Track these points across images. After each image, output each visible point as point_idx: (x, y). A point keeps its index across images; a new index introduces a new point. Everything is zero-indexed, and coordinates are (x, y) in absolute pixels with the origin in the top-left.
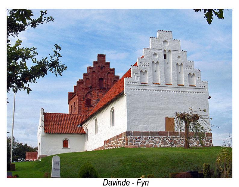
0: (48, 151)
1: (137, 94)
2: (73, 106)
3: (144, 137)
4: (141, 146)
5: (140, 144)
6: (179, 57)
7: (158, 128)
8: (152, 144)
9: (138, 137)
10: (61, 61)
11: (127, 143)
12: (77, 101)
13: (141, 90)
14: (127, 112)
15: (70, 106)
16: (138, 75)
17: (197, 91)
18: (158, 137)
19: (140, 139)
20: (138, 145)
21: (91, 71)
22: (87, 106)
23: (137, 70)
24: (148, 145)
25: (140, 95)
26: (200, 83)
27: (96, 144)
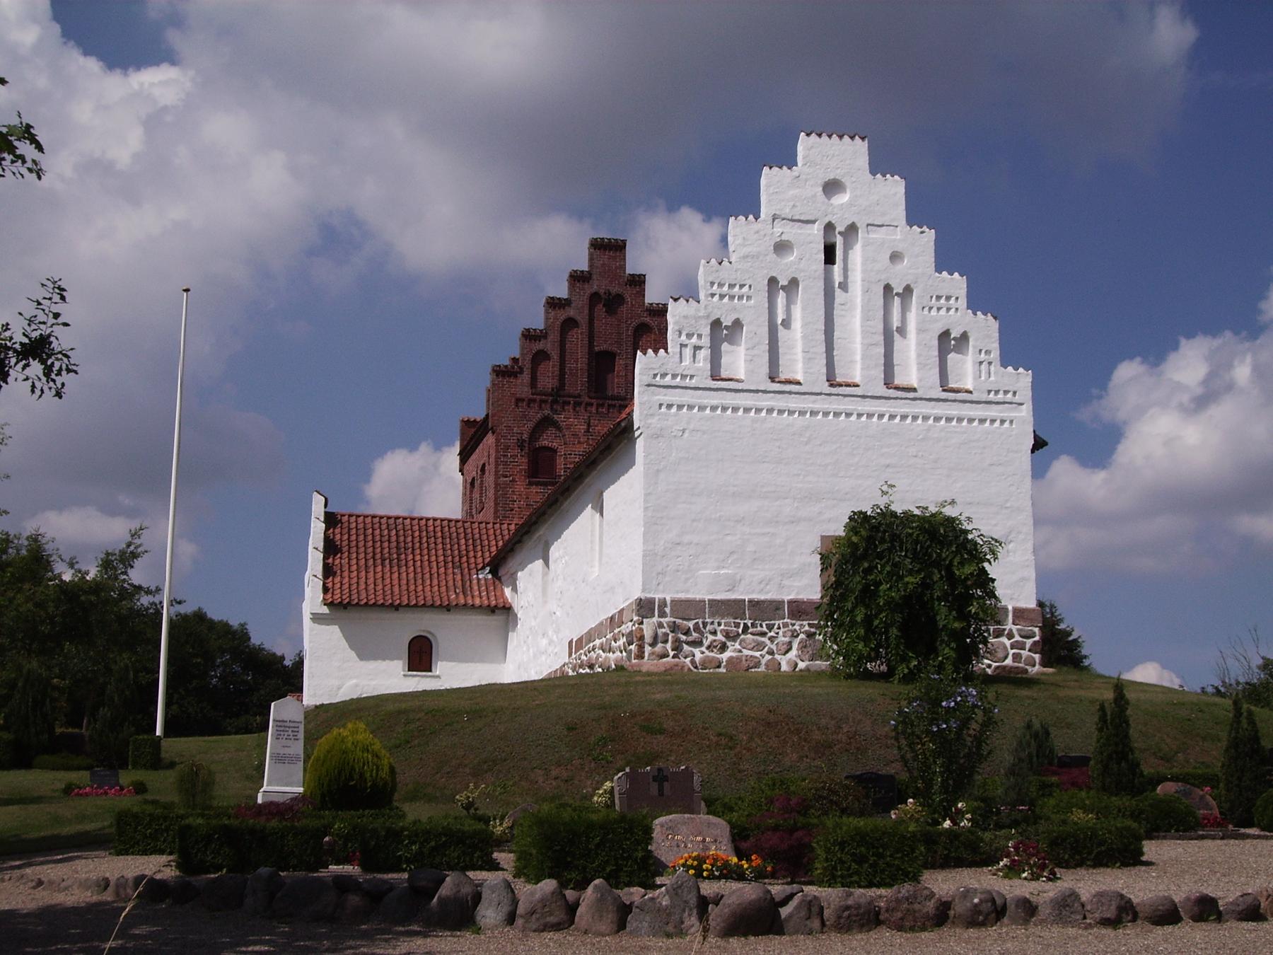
0: (339, 688)
1: (691, 427)
2: (477, 483)
3: (719, 624)
4: (705, 664)
5: (698, 656)
6: (895, 257)
7: (786, 582)
8: (757, 654)
9: (691, 624)
10: (62, 340)
11: (641, 648)
12: (492, 460)
13: (714, 408)
14: (646, 509)
15: (465, 481)
16: (700, 343)
17: (978, 411)
18: (785, 625)
19: (702, 634)
20: (693, 662)
21: (556, 318)
22: (537, 484)
23: (697, 318)
24: (737, 658)
25: (704, 433)
26: (992, 378)
27: (543, 658)
